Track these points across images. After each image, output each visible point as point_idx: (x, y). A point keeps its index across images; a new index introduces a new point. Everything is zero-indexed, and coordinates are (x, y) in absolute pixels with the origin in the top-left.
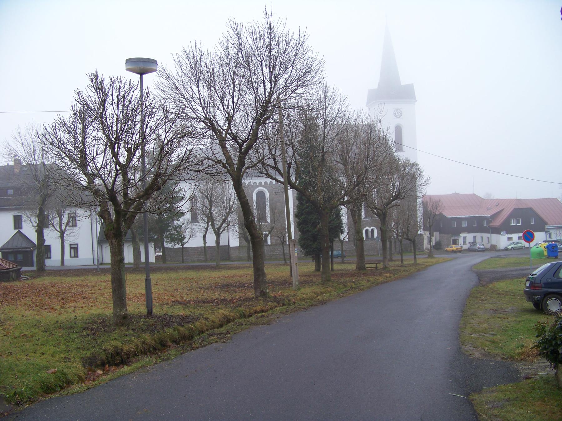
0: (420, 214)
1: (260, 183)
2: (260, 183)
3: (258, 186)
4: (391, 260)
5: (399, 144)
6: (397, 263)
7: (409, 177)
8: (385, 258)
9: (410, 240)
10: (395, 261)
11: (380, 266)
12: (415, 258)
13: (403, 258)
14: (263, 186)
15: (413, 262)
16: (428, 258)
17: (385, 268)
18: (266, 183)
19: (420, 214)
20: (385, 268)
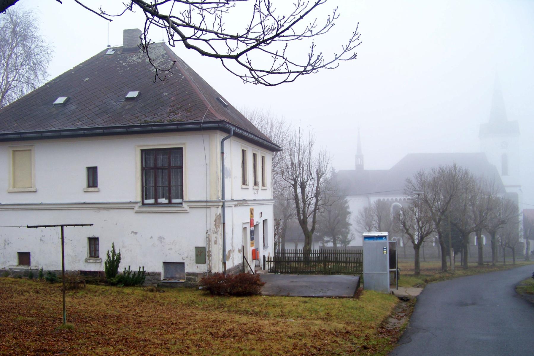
0: (521, 227)
1: (396, 199)
2: (396, 199)
3: (394, 202)
4: (497, 262)
5: (505, 172)
6: (501, 263)
7: (511, 207)
8: (493, 259)
9: (511, 248)
10: (499, 262)
11: (490, 264)
12: (514, 260)
13: (230, 199)
14: (398, 202)
15: (512, 263)
16: (450, 257)
17: (494, 265)
18: (400, 199)
19: (521, 227)
20: (494, 265)
